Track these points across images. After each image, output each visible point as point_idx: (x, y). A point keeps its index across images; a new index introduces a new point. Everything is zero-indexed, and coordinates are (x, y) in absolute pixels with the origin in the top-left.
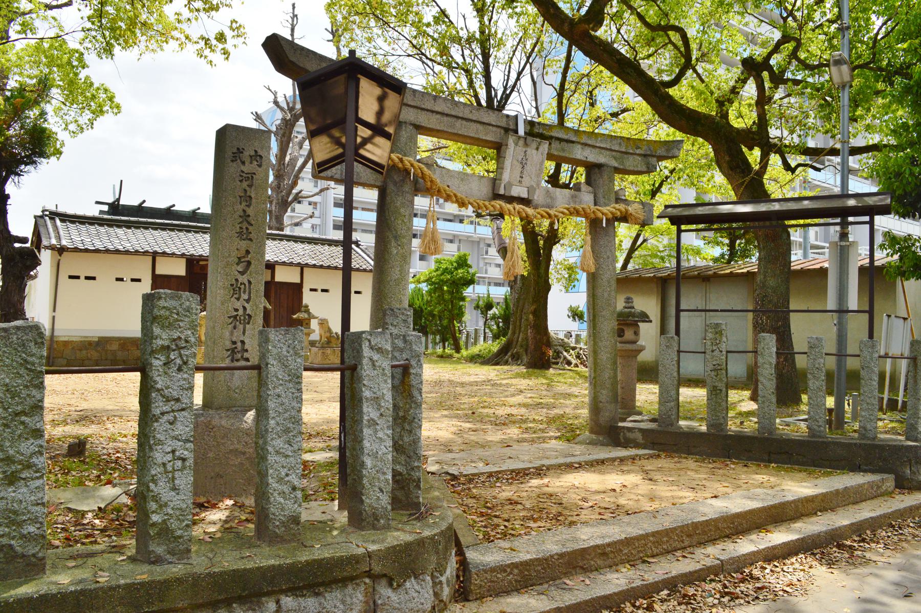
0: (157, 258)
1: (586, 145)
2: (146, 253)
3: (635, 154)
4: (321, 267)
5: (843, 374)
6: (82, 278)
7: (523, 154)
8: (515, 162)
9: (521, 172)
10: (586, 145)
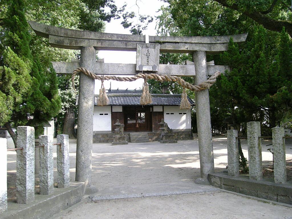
0: (164, 106)
1: (186, 43)
2: (161, 105)
3: (217, 43)
4: (169, 105)
5: (262, 137)
6: (104, 114)
7: (147, 51)
8: (143, 55)
9: (148, 60)
10: (186, 43)
